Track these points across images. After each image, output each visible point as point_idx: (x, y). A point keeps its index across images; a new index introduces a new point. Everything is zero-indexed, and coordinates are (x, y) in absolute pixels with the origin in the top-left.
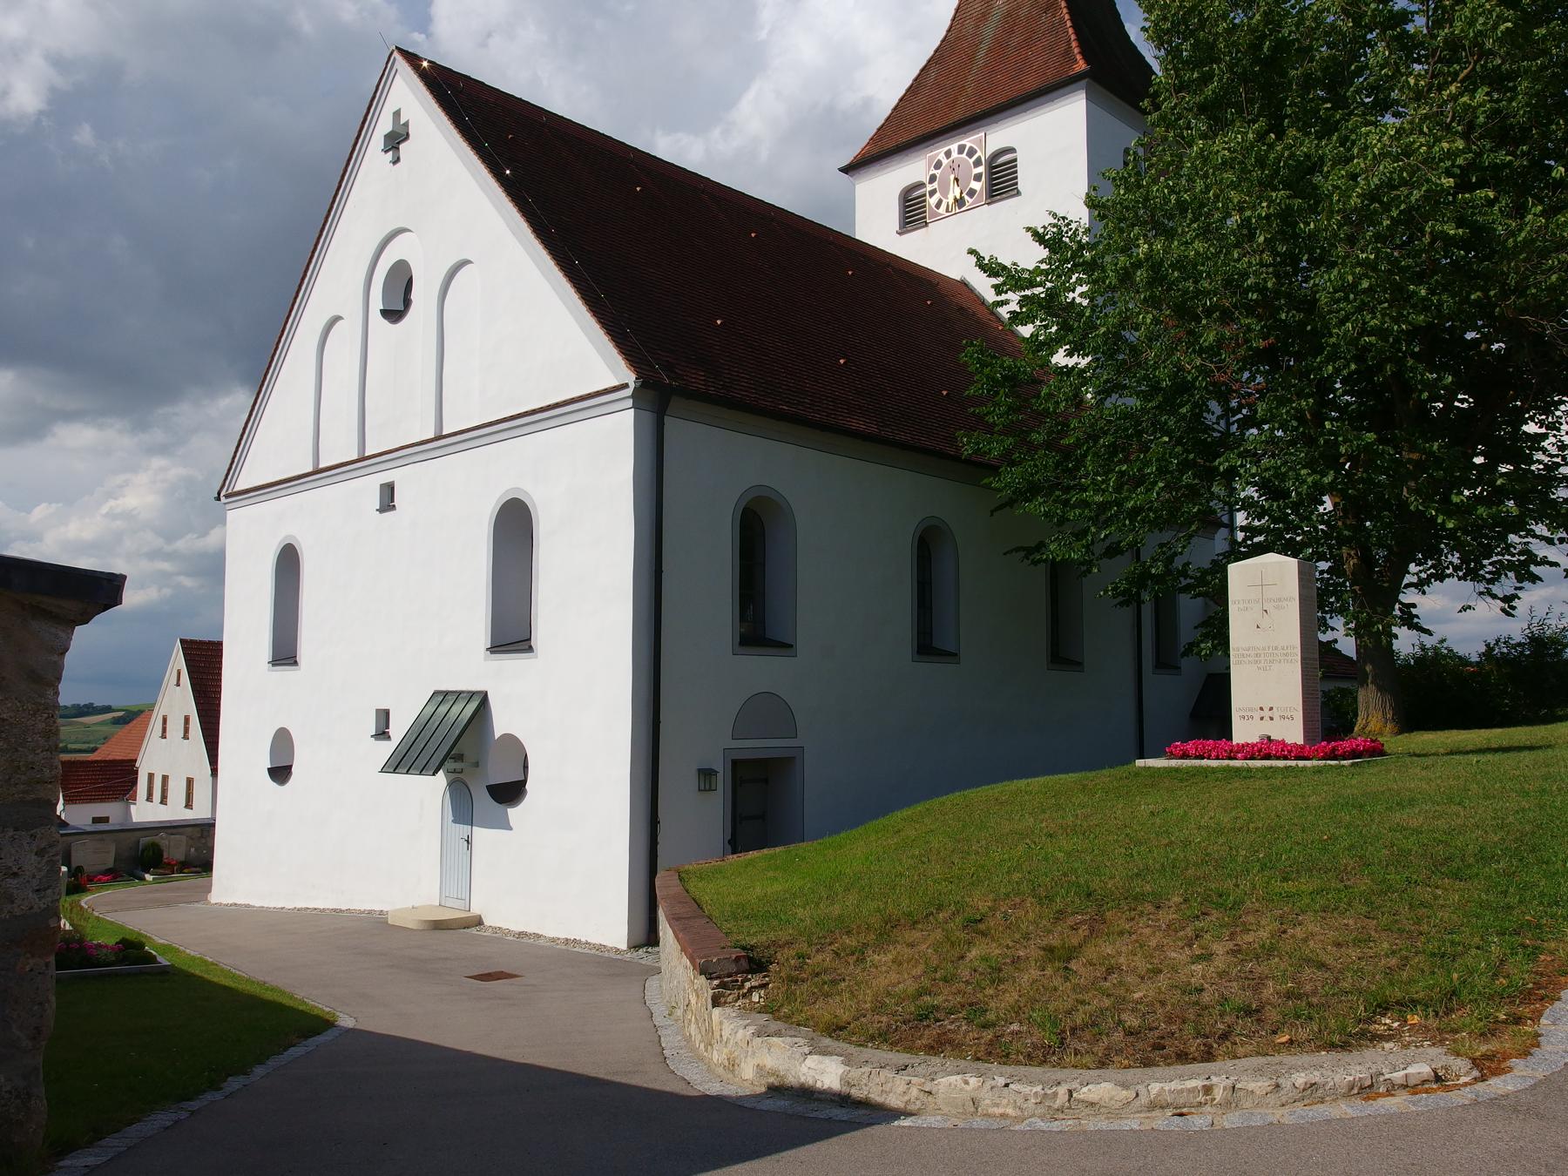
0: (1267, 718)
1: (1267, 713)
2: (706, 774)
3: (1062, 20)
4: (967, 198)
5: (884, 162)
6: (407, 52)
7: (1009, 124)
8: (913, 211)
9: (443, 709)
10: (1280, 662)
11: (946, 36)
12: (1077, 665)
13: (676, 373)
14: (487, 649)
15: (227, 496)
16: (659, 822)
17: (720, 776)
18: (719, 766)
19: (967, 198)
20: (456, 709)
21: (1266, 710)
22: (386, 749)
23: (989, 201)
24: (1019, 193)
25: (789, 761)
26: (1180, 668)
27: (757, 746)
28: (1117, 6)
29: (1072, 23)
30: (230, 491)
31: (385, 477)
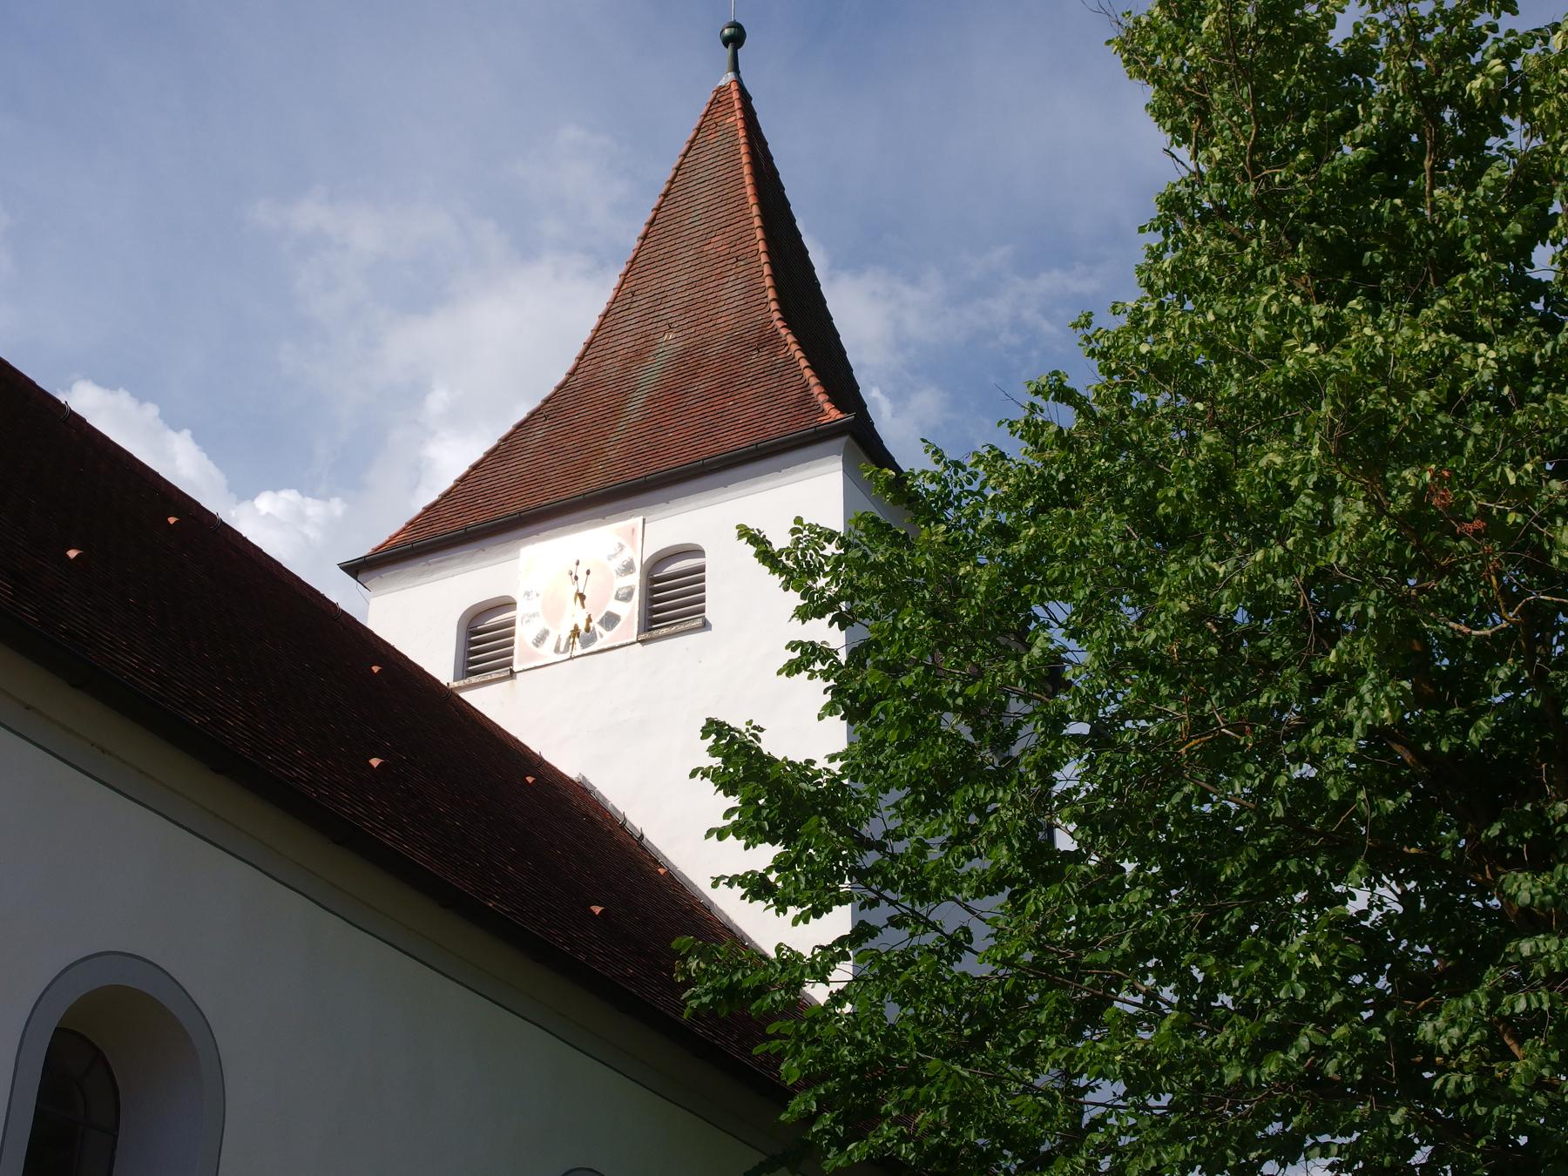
3: (790, 361)
4: (599, 629)
5: (433, 559)
7: (686, 507)
11: (566, 382)
19: (599, 629)
23: (642, 637)
24: (705, 626)
29: (809, 361)
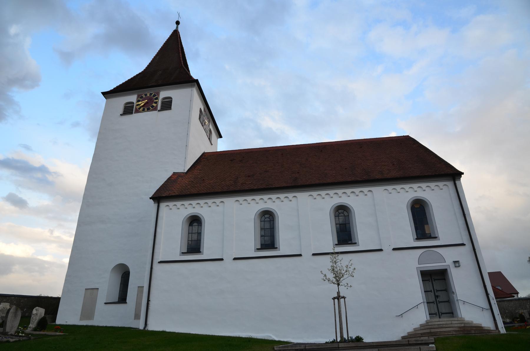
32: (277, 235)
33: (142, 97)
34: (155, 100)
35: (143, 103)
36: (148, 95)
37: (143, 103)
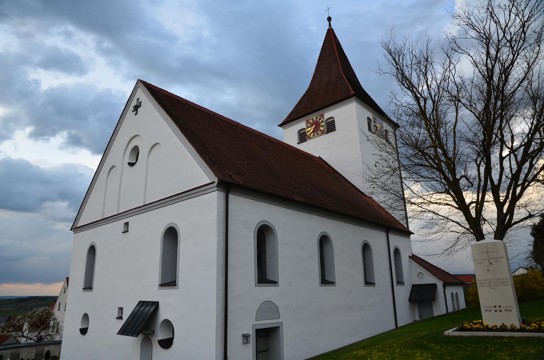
0: (498, 311)
1: (498, 308)
2: (246, 337)
6: (143, 81)
8: (303, 137)
9: (142, 308)
10: (501, 285)
12: (373, 284)
13: (233, 178)
14: (159, 285)
15: (74, 229)
16: (228, 358)
17: (251, 337)
18: (251, 332)
20: (147, 309)
21: (497, 307)
22: (121, 323)
25: (278, 327)
26: (404, 283)
27: (266, 323)
28: (359, 80)
30: (75, 227)
31: (126, 220)
32: (297, 122)
33: (310, 123)
34: (320, 121)
35: (312, 129)
36: (315, 119)
37: (312, 129)
